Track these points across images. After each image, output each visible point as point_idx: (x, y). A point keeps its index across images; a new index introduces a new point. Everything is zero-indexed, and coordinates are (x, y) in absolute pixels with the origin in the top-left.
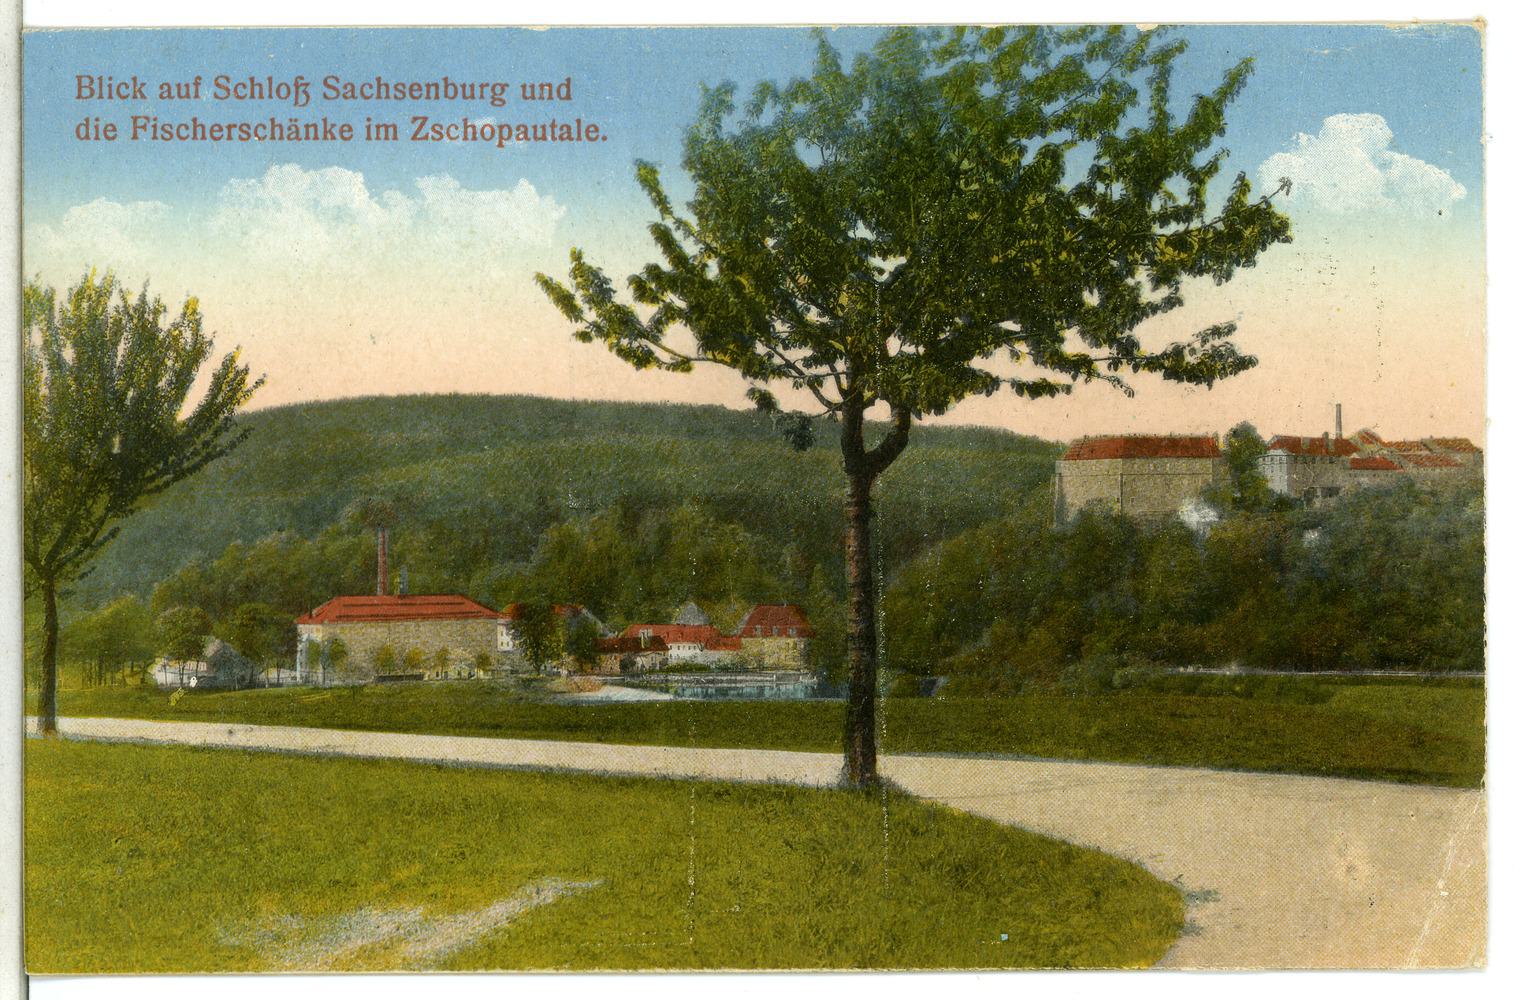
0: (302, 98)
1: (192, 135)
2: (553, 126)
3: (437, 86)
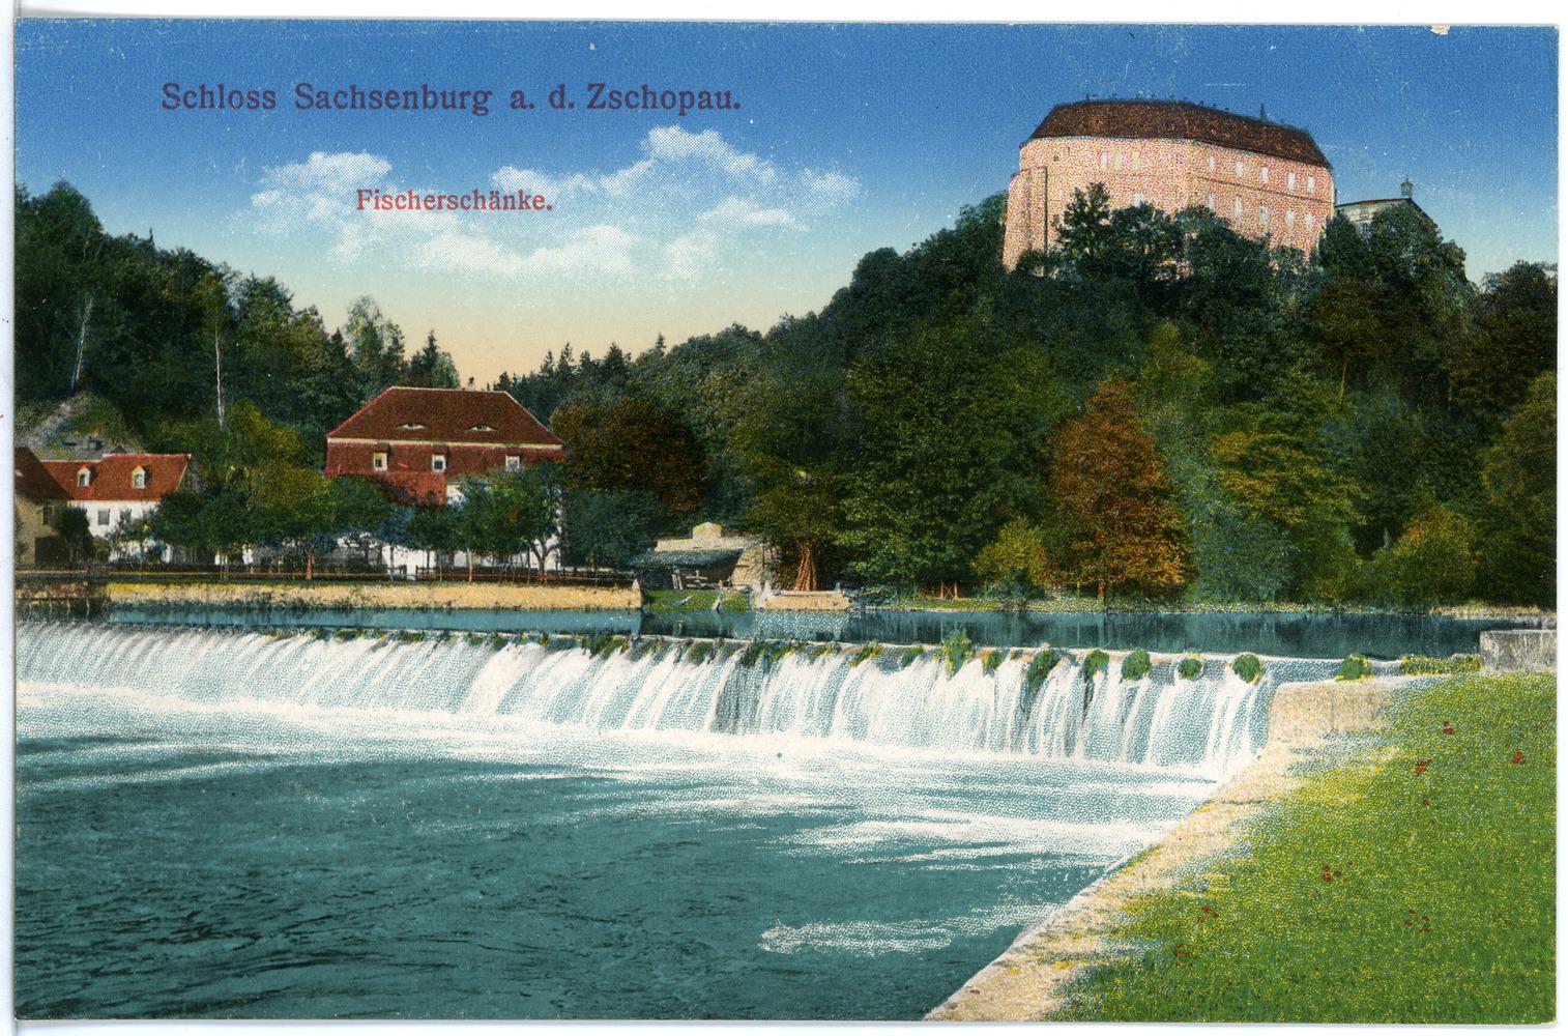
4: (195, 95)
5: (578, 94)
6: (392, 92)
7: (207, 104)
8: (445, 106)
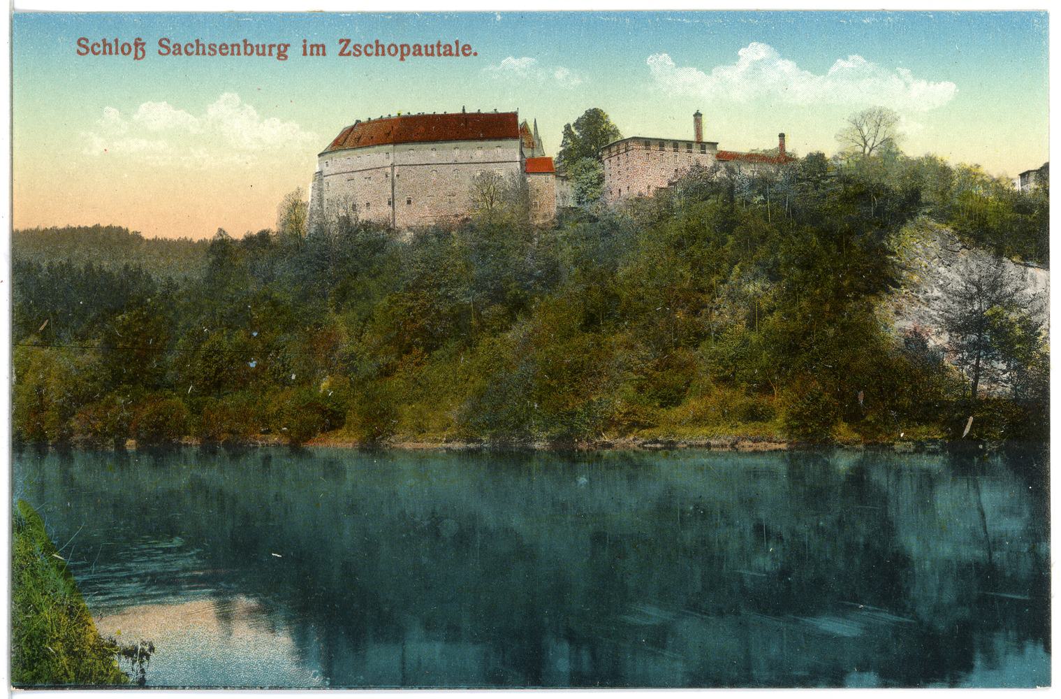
0: (140, 54)
2: (439, 46)
5: (333, 48)
6: (224, 44)
8: (258, 54)
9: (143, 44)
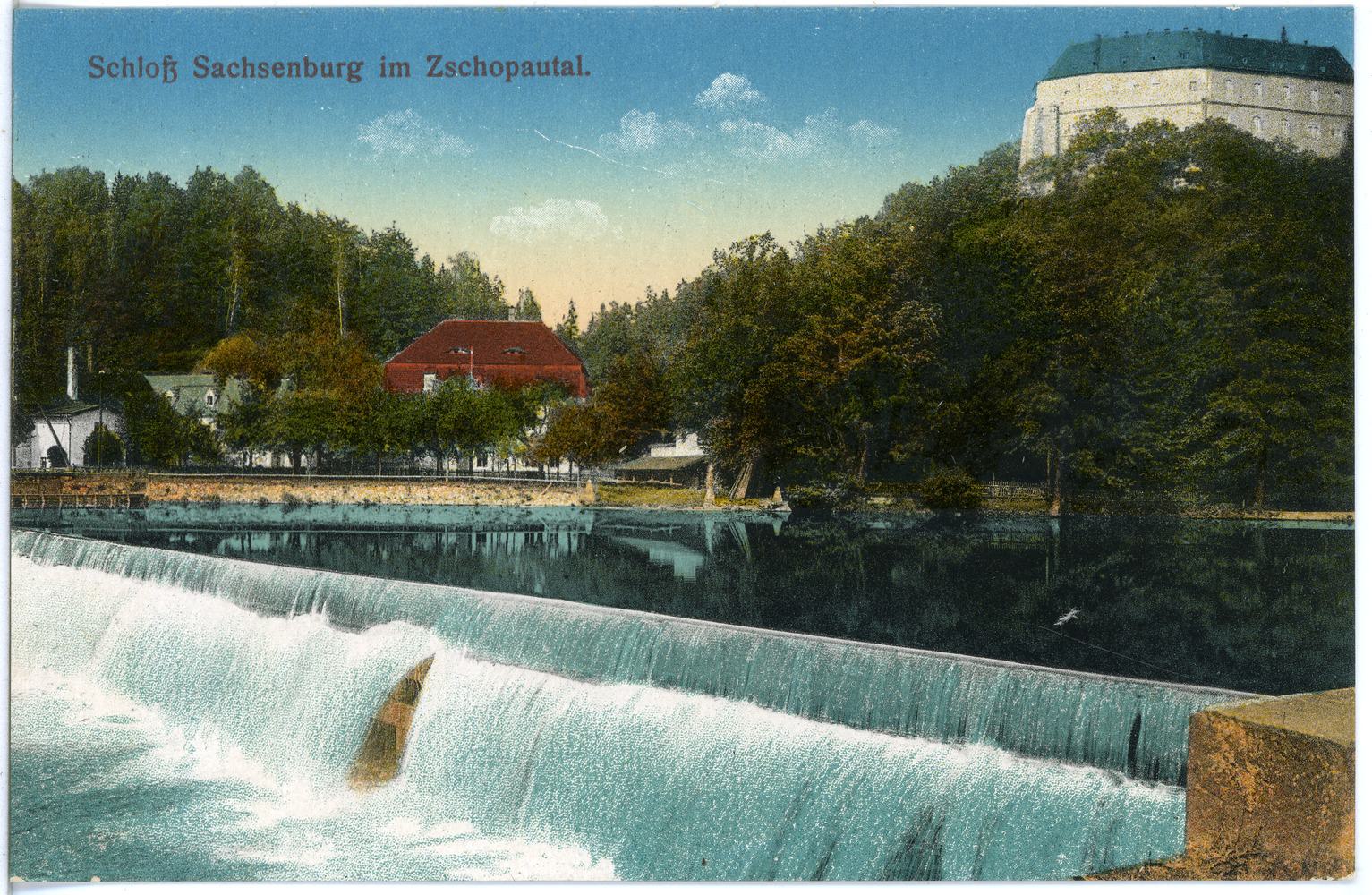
0: (170, 75)
1: (242, 73)
2: (556, 62)
3: (298, 65)
4: (469, 65)
7: (480, 72)
9: (174, 63)
